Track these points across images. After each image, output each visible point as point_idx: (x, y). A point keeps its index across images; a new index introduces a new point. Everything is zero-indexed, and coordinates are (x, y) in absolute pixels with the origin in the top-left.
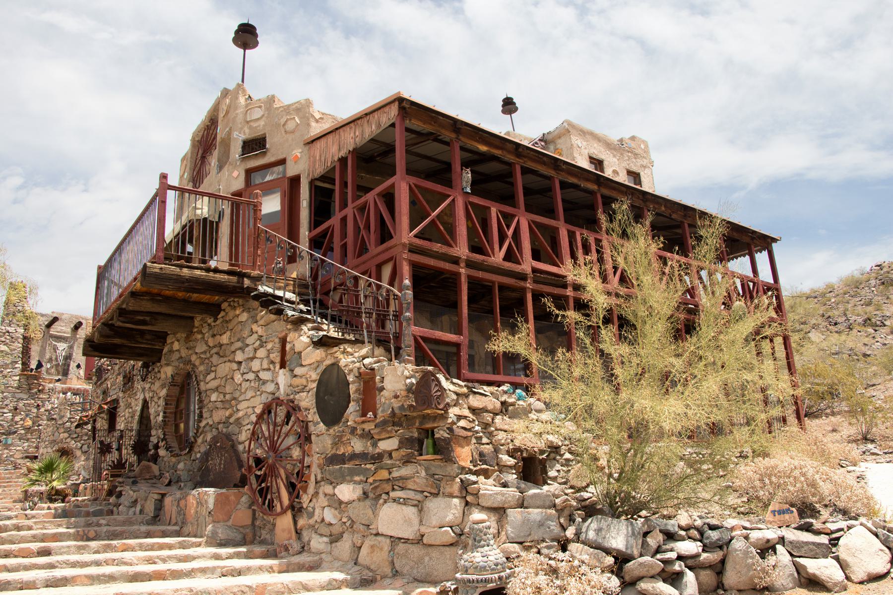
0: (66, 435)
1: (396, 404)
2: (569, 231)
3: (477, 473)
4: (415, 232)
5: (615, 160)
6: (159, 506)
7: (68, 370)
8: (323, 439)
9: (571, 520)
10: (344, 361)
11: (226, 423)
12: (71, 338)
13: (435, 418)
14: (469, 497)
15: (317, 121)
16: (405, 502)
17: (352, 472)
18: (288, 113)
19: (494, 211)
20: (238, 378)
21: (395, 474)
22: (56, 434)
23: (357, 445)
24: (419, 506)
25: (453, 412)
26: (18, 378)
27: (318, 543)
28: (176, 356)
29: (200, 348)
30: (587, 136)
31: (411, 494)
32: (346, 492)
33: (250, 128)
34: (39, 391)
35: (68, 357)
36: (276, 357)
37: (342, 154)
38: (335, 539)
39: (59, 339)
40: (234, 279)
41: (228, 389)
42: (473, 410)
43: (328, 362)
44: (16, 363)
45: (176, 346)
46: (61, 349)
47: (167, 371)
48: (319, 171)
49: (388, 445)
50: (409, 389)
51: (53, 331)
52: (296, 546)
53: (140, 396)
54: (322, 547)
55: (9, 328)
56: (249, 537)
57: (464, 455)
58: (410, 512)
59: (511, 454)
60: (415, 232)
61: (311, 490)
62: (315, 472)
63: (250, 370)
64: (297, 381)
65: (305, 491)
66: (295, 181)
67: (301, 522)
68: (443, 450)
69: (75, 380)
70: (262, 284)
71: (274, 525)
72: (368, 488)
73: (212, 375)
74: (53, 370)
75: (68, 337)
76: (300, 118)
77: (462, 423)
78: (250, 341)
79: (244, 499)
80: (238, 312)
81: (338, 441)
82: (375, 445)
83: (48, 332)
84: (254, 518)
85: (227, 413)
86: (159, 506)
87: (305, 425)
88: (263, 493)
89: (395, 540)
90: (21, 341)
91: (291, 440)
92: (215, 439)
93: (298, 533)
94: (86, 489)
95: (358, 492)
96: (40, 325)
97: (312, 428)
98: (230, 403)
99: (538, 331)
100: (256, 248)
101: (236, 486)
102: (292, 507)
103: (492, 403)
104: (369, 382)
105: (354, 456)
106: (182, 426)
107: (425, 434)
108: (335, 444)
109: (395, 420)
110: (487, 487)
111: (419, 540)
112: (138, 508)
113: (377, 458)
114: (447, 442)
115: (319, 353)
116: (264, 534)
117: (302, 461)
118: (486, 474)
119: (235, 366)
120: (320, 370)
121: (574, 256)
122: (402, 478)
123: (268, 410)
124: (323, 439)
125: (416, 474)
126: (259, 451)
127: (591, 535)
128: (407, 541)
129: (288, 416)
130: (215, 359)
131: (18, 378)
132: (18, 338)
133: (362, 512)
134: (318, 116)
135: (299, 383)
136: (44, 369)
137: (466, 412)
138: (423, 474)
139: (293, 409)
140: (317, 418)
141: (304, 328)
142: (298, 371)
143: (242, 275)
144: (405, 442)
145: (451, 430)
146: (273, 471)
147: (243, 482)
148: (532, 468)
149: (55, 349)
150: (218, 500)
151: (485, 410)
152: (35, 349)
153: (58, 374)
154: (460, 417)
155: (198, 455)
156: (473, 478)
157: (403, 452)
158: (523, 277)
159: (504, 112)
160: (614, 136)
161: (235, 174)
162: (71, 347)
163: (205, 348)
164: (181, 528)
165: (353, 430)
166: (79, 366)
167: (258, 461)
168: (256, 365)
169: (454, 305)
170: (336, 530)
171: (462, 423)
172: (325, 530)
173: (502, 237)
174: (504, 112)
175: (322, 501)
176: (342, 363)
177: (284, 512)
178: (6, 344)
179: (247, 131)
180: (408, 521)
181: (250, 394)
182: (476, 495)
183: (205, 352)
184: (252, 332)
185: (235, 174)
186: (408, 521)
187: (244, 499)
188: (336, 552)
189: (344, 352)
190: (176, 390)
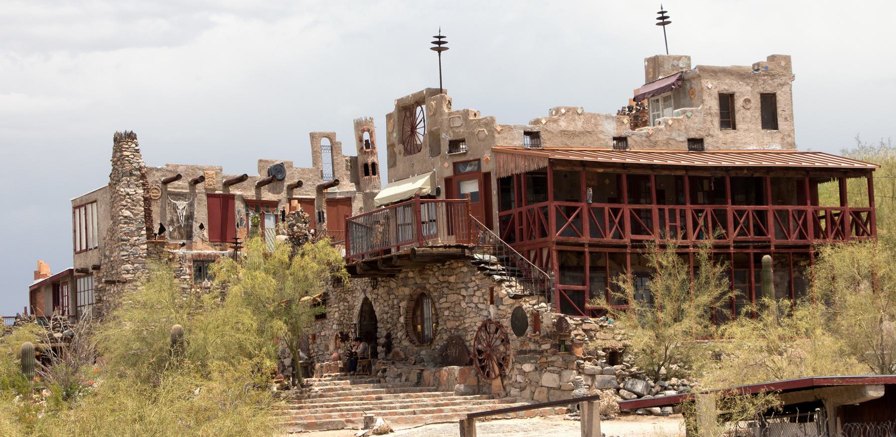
2: (659, 209)
3: (585, 360)
5: (749, 88)
6: (420, 375)
7: (191, 232)
8: (515, 342)
9: (623, 380)
10: (525, 306)
11: (457, 329)
12: (190, 193)
13: (565, 336)
15: (499, 133)
16: (553, 372)
17: (530, 359)
18: (480, 126)
19: (606, 208)
20: (463, 305)
21: (549, 360)
23: (532, 346)
24: (560, 374)
25: (573, 333)
26: (145, 246)
27: (514, 392)
28: (411, 282)
29: (433, 281)
30: (719, 74)
31: (556, 368)
32: (527, 367)
33: (454, 132)
34: (170, 260)
35: (190, 217)
36: (488, 297)
37: (518, 172)
38: (522, 389)
39: (179, 196)
40: (459, 250)
41: (457, 309)
42: (584, 330)
43: (517, 305)
44: (141, 229)
46: (181, 208)
49: (546, 346)
50: (554, 324)
51: (171, 188)
52: (504, 394)
54: (516, 393)
55: (128, 190)
56: (477, 391)
57: (579, 352)
58: (556, 376)
59: (604, 350)
61: (510, 366)
62: (512, 358)
63: (472, 302)
64: (500, 312)
65: (507, 366)
66: (487, 176)
67: (505, 382)
68: (569, 350)
69: (200, 244)
70: (476, 253)
71: (491, 385)
72: (538, 366)
73: (444, 300)
74: (176, 234)
75: (186, 193)
76: (488, 131)
77: (578, 337)
78: (470, 285)
79: (473, 371)
81: (523, 343)
82: (540, 346)
83: (166, 190)
84: (479, 381)
85: (457, 324)
86: (420, 375)
87: (506, 335)
88: (483, 368)
89: (549, 388)
90: (142, 203)
91: (498, 342)
92: (451, 339)
93: (504, 388)
94: (322, 367)
95: (533, 368)
96: (157, 182)
97: (510, 337)
98: (461, 317)
100: (469, 229)
101: (467, 365)
102: (501, 375)
103: (595, 326)
104: (536, 316)
105: (530, 351)
106: (419, 327)
107: (561, 341)
108: (521, 345)
109: (548, 336)
110: (588, 365)
111: (559, 388)
112: (403, 378)
113: (541, 352)
114: (571, 346)
115: (512, 301)
116: (485, 389)
117: (505, 353)
118: (590, 360)
119: (461, 298)
120: (513, 308)
121: (662, 226)
122: (552, 361)
123: (484, 326)
124: (515, 342)
125: (558, 359)
126: (480, 347)
127: (629, 386)
128: (554, 388)
129: (497, 330)
130: (445, 290)
131: (145, 246)
132: (139, 200)
133: (535, 376)
134: (499, 129)
135: (503, 313)
136: (167, 232)
137: (581, 332)
139: (499, 327)
140: (512, 332)
141: (503, 285)
142: (501, 307)
143: (464, 248)
144: (553, 346)
145: (572, 341)
146: (489, 357)
147: (471, 363)
148: (614, 357)
149: (175, 208)
150: (462, 373)
151: (591, 330)
152: (155, 209)
153: (182, 238)
154: (576, 335)
156: (582, 362)
157: (552, 350)
158: (625, 247)
160: (747, 62)
161: (446, 165)
162: (191, 205)
163: (436, 281)
164: (437, 386)
165: (530, 339)
166: (202, 227)
167: (480, 352)
168: (475, 300)
170: (523, 385)
171: (578, 337)
172: (517, 385)
173: (612, 222)
175: (516, 371)
176: (524, 306)
177: (496, 377)
178: (128, 209)
179: (452, 134)
180: (554, 380)
181: (472, 315)
182: (583, 369)
183: (437, 284)
185: (446, 165)
186: (554, 380)
187: (473, 371)
188: (523, 395)
189: (525, 301)
190: (413, 304)
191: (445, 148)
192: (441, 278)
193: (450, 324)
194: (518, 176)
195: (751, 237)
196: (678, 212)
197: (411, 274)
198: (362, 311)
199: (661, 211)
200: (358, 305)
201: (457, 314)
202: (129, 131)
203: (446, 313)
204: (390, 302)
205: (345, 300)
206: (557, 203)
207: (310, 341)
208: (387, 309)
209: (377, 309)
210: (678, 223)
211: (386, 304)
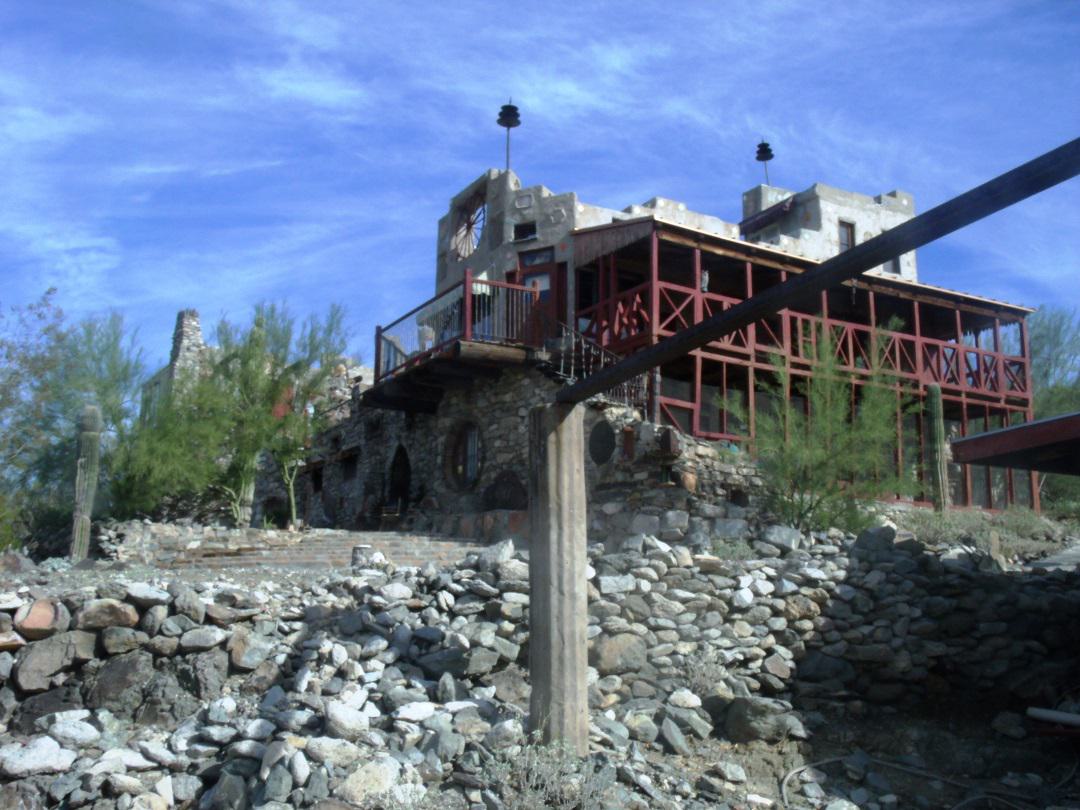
0: (276, 484)
1: (648, 449)
4: (664, 325)
14: (691, 508)
17: (616, 495)
21: (646, 495)
22: (265, 484)
23: (619, 477)
29: (482, 403)
37: (605, 252)
45: (454, 401)
47: (446, 422)
48: (585, 261)
49: (641, 476)
50: (656, 439)
53: (394, 444)
60: (664, 325)
66: (563, 266)
73: (494, 427)
80: (519, 377)
81: (605, 474)
82: (632, 476)
99: (835, 382)
105: (616, 484)
106: (460, 468)
113: (633, 485)
119: (519, 420)
130: (498, 414)
138: (664, 495)
144: (651, 475)
155: (482, 490)
157: (652, 480)
158: (746, 357)
159: (759, 158)
165: (617, 467)
169: (691, 378)
174: (759, 158)
184: (534, 394)
185: (509, 255)
191: (510, 235)
192: (493, 400)
193: (502, 458)
194: (605, 258)
195: (898, 372)
196: (813, 327)
197: (454, 401)
198: (395, 463)
199: (793, 320)
200: (391, 454)
201: (511, 443)
202: (192, 308)
203: (498, 443)
204: (427, 446)
205: (378, 453)
206: (663, 284)
207: (338, 506)
208: (422, 455)
209: (412, 457)
210: (813, 339)
211: (422, 449)
